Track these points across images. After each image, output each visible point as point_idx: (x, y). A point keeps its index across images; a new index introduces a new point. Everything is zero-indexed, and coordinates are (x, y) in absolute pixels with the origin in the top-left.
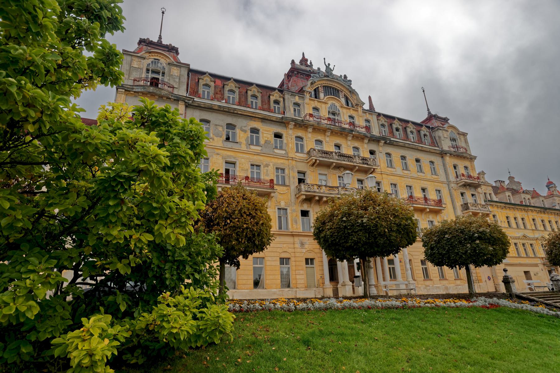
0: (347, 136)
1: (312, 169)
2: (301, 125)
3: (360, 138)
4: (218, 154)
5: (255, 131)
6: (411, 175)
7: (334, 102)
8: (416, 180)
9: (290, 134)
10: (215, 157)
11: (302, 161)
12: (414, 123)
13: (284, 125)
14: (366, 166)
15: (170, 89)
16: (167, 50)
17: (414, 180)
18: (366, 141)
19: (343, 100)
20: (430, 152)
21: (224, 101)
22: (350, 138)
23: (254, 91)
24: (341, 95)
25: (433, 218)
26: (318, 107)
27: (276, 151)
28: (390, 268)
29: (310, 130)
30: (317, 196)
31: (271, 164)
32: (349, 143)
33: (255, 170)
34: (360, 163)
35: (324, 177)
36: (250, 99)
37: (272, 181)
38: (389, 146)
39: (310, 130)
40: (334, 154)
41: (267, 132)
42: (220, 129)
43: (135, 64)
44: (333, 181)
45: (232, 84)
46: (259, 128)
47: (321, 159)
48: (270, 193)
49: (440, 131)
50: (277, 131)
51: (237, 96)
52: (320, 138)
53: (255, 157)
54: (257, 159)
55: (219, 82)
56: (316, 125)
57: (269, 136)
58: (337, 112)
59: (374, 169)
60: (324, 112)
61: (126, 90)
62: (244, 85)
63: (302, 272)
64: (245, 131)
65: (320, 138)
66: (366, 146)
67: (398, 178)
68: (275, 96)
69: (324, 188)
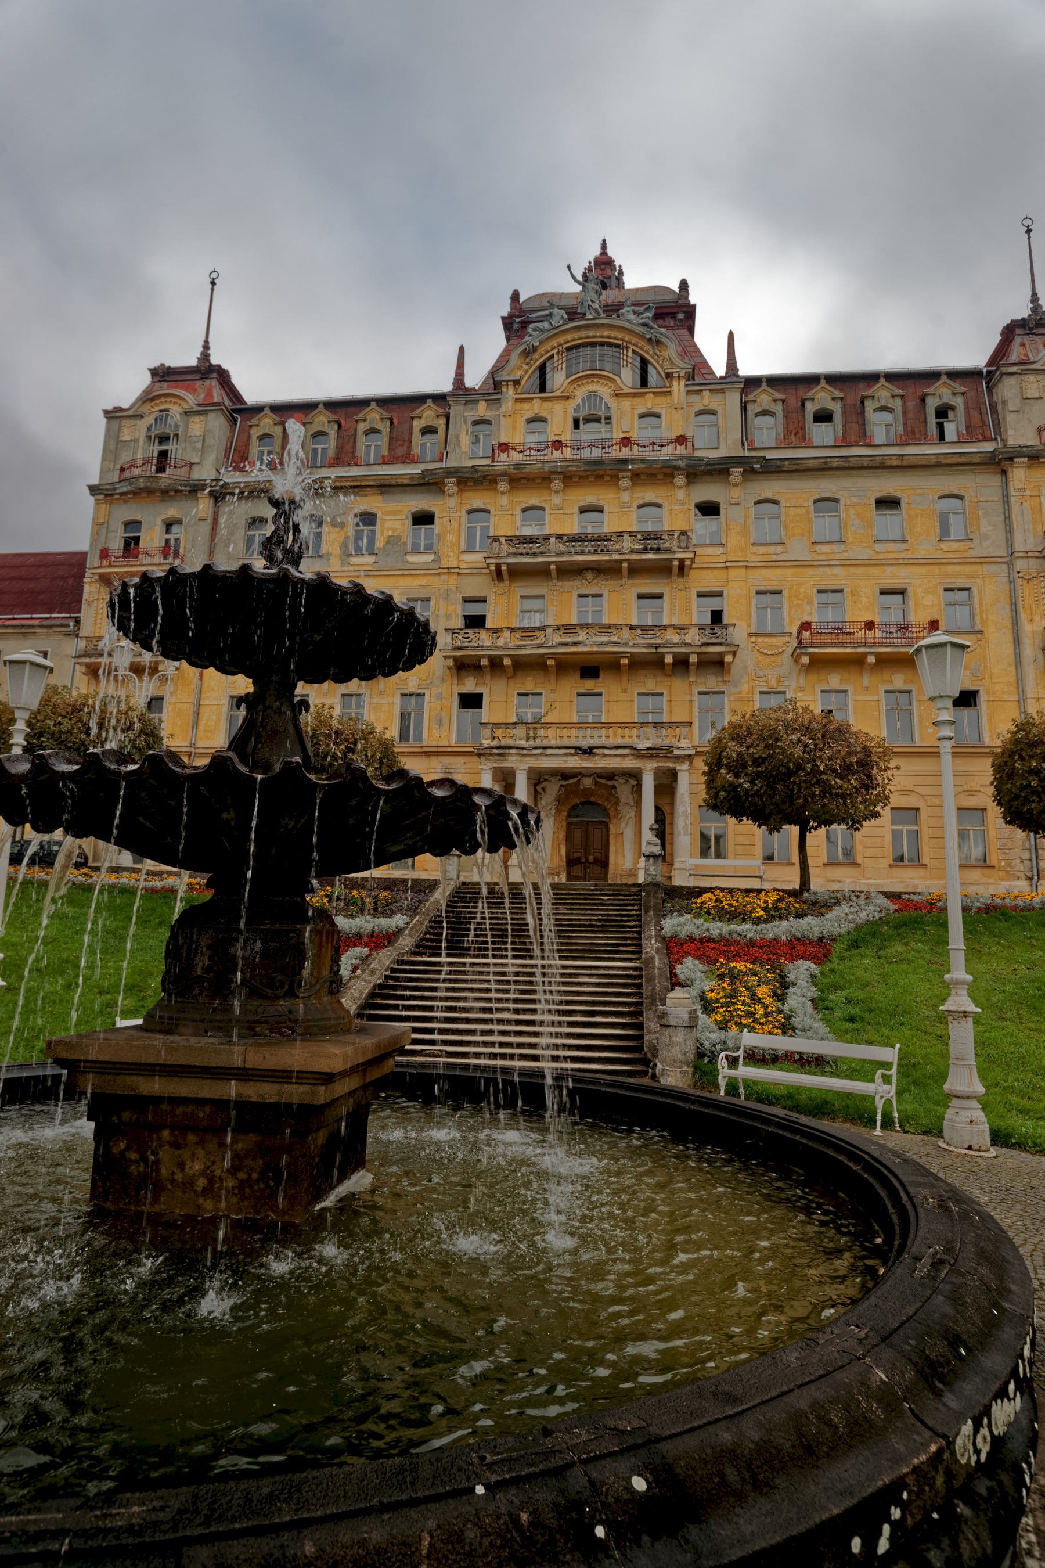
0: (615, 478)
1: (503, 586)
2: (472, 480)
3: (660, 474)
5: (368, 518)
6: (846, 555)
8: (862, 570)
9: (450, 508)
11: (474, 572)
13: (433, 488)
14: (651, 556)
16: (198, 376)
17: (853, 570)
18: (680, 480)
19: (628, 377)
20: (938, 465)
22: (625, 483)
23: (373, 420)
26: (544, 414)
27: (411, 558)
29: (503, 486)
30: (483, 656)
32: (626, 497)
34: (633, 551)
35: (536, 604)
38: (763, 477)
39: (503, 486)
40: (553, 540)
46: (374, 511)
47: (511, 560)
49: (1011, 381)
50: (419, 508)
55: (912, 390)
56: (512, 471)
58: (602, 414)
59: (682, 561)
60: (559, 422)
61: (106, 495)
64: (343, 525)
66: (681, 494)
67: (789, 572)
68: (267, 423)
69: (507, 634)
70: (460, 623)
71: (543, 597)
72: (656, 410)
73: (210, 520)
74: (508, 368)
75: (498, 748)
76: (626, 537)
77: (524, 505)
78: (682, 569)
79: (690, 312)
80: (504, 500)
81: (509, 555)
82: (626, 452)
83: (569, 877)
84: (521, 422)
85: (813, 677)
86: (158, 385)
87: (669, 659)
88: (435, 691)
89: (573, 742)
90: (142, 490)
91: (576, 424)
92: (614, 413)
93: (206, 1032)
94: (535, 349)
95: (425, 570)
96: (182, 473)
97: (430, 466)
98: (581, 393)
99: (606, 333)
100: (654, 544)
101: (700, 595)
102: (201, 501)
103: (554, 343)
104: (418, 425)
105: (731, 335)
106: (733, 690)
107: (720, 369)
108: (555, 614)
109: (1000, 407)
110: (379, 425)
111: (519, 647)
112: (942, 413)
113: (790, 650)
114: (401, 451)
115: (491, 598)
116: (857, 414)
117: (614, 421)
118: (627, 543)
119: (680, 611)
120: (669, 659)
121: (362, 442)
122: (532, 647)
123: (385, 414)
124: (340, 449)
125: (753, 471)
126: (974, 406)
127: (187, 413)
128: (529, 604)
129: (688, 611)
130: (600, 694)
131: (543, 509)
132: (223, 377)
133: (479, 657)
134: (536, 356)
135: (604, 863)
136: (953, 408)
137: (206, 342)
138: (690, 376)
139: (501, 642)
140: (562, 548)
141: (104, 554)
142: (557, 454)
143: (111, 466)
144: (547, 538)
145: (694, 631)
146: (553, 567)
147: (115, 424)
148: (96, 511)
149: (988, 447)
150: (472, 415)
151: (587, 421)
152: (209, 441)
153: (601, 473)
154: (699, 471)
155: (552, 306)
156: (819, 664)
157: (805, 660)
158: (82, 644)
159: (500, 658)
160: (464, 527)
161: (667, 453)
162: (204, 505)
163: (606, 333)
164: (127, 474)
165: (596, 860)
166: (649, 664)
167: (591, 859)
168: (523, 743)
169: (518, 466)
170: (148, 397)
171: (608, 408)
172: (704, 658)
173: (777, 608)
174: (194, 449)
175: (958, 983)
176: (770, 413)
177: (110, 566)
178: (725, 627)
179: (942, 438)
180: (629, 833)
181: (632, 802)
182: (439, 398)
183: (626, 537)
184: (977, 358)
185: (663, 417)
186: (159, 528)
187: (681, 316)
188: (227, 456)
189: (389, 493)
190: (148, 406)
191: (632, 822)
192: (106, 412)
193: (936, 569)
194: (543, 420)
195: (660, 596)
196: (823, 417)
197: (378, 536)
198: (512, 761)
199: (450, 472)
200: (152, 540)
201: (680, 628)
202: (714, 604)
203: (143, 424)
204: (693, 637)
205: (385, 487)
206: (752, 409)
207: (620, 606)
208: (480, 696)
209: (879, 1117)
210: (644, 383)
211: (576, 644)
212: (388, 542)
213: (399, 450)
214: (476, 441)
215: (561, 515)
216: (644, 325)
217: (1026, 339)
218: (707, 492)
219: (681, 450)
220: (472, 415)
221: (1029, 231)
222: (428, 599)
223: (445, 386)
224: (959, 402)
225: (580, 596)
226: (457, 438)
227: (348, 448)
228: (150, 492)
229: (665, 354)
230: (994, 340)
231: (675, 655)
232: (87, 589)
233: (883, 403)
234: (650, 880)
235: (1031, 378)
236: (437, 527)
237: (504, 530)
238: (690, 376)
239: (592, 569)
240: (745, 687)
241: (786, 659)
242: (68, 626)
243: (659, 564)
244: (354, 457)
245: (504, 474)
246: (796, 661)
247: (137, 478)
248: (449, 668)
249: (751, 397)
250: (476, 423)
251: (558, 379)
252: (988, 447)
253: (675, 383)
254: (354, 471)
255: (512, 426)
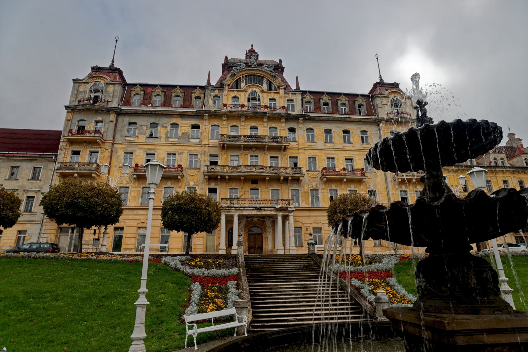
2: (214, 115)
3: (277, 118)
4: (141, 149)
6: (335, 147)
7: (254, 89)
8: (339, 152)
9: (205, 125)
10: (138, 151)
11: (214, 146)
12: (363, 96)
14: (275, 144)
15: (105, 104)
18: (243, 119)
19: (265, 86)
21: (150, 105)
22: (265, 120)
23: (178, 92)
24: (265, 81)
25: (355, 187)
26: (238, 96)
27: (191, 140)
28: (295, 236)
31: (186, 152)
32: (266, 124)
33: (350, 164)
34: (269, 142)
35: (236, 158)
36: (322, 107)
37: (363, 169)
39: (224, 118)
40: (242, 137)
41: (185, 125)
42: (145, 128)
43: (81, 89)
44: (268, 162)
45: (360, 100)
47: (228, 143)
48: (362, 179)
49: (379, 99)
51: (312, 106)
52: (273, 125)
53: (172, 148)
54: (172, 149)
56: (228, 113)
57: (186, 128)
58: (257, 97)
59: (285, 146)
60: (243, 99)
61: (72, 110)
62: (168, 88)
63: (201, 239)
64: (166, 127)
65: (273, 125)
66: (283, 125)
67: (318, 151)
69: (227, 168)
70: (208, 164)
71: (238, 156)
72: (275, 98)
73: (114, 122)
74: (226, 80)
75: (228, 207)
76: (267, 137)
77: (231, 125)
78: (285, 149)
79: (283, 69)
80: (225, 123)
81: (227, 141)
82: (266, 110)
83: (249, 253)
84: (230, 98)
85: (327, 185)
86: (94, 73)
87: (282, 178)
88: (200, 187)
89: (254, 205)
90: (87, 109)
91: (249, 100)
92: (261, 97)
93: (494, 312)
94: (235, 75)
95: (196, 145)
96: (105, 104)
97: (198, 110)
98: (250, 90)
99: (258, 72)
100: (276, 140)
101: (290, 158)
102: (111, 115)
103: (241, 74)
104: (194, 95)
105: (209, 72)
106: (302, 189)
107: (294, 87)
108: (242, 161)
109: (376, 106)
110: (180, 94)
111: (231, 172)
112: (360, 106)
113: (319, 176)
114: (187, 104)
115: (220, 155)
116: (335, 104)
117: (261, 100)
118: (267, 140)
119: (284, 162)
120: (282, 178)
121: (154, 98)
122: (236, 172)
123: (182, 91)
124: (165, 101)
125: (306, 119)
126: (368, 105)
127: (107, 84)
128: (233, 158)
129: (287, 163)
130: (258, 189)
131: (238, 127)
132: (120, 72)
133: (218, 175)
134: (235, 77)
135: (261, 248)
136: (363, 105)
137: (113, 60)
138: (285, 88)
139: (225, 170)
140: (246, 140)
141: (71, 131)
142: (243, 109)
143: (75, 99)
144: (240, 136)
145: (290, 169)
146: (242, 146)
147: (77, 85)
148: (67, 115)
149: (374, 117)
150: (213, 94)
151: (252, 99)
152: (116, 94)
153: (257, 116)
154: (289, 118)
155: (241, 62)
156: (330, 181)
157: (325, 179)
158: (58, 165)
159: (225, 176)
160: (210, 131)
161: (279, 111)
162: (113, 117)
163: (258, 72)
164: (81, 103)
165: (259, 247)
166: (276, 179)
167: (257, 246)
168: (236, 205)
169: (230, 112)
170: (91, 76)
171: (259, 96)
172: (294, 178)
173: (131, 159)
174: (109, 96)
175: (503, 281)
176: (180, 96)
177: (72, 136)
178: (300, 168)
179: (360, 114)
180: (270, 237)
181: (271, 226)
182: (202, 88)
183: (267, 137)
184: (366, 92)
185: (277, 100)
186: (93, 124)
187: (280, 70)
188: (122, 100)
189: (183, 117)
190: (90, 80)
191: (271, 233)
192: (73, 80)
193: (361, 152)
194: (238, 98)
195: (277, 157)
196: (326, 104)
197: (179, 131)
198: (232, 212)
199: (206, 112)
200: (90, 127)
201: (286, 168)
202: (294, 161)
203: (88, 86)
204: (290, 171)
205: (182, 115)
206: (305, 100)
207: (264, 160)
208: (216, 189)
209: (195, 341)
210: (270, 89)
211: (252, 172)
212: (183, 134)
213: (167, 103)
214: (215, 102)
215: (244, 129)
216: (271, 71)
217: (381, 88)
218: (292, 125)
219: (284, 111)
220: (213, 94)
221: (377, 58)
222: (197, 155)
223: (204, 84)
224: (364, 103)
225: (251, 156)
226: (208, 101)
227: (168, 101)
228: (90, 110)
229: (278, 81)
230: (371, 87)
231: (284, 177)
232: (61, 144)
233: (343, 102)
234: (311, 252)
235: (384, 99)
236: (201, 130)
237: (225, 133)
238: (285, 88)
239: (255, 147)
240: (306, 188)
241: (318, 179)
242: (52, 158)
243: (278, 147)
244: (170, 104)
245: (225, 114)
246: (322, 180)
247: (86, 105)
248: (206, 179)
249: (304, 96)
250: (214, 97)
251: (243, 85)
252: (374, 117)
253: (281, 90)
254: (171, 109)
255: (227, 98)
